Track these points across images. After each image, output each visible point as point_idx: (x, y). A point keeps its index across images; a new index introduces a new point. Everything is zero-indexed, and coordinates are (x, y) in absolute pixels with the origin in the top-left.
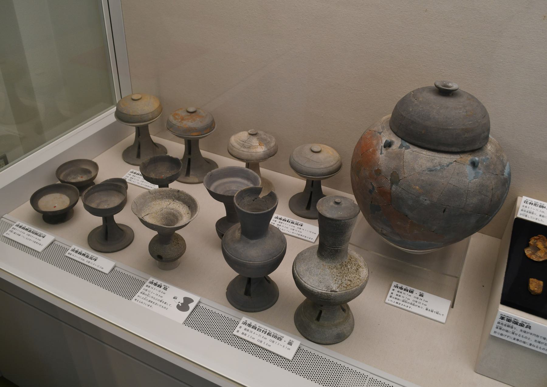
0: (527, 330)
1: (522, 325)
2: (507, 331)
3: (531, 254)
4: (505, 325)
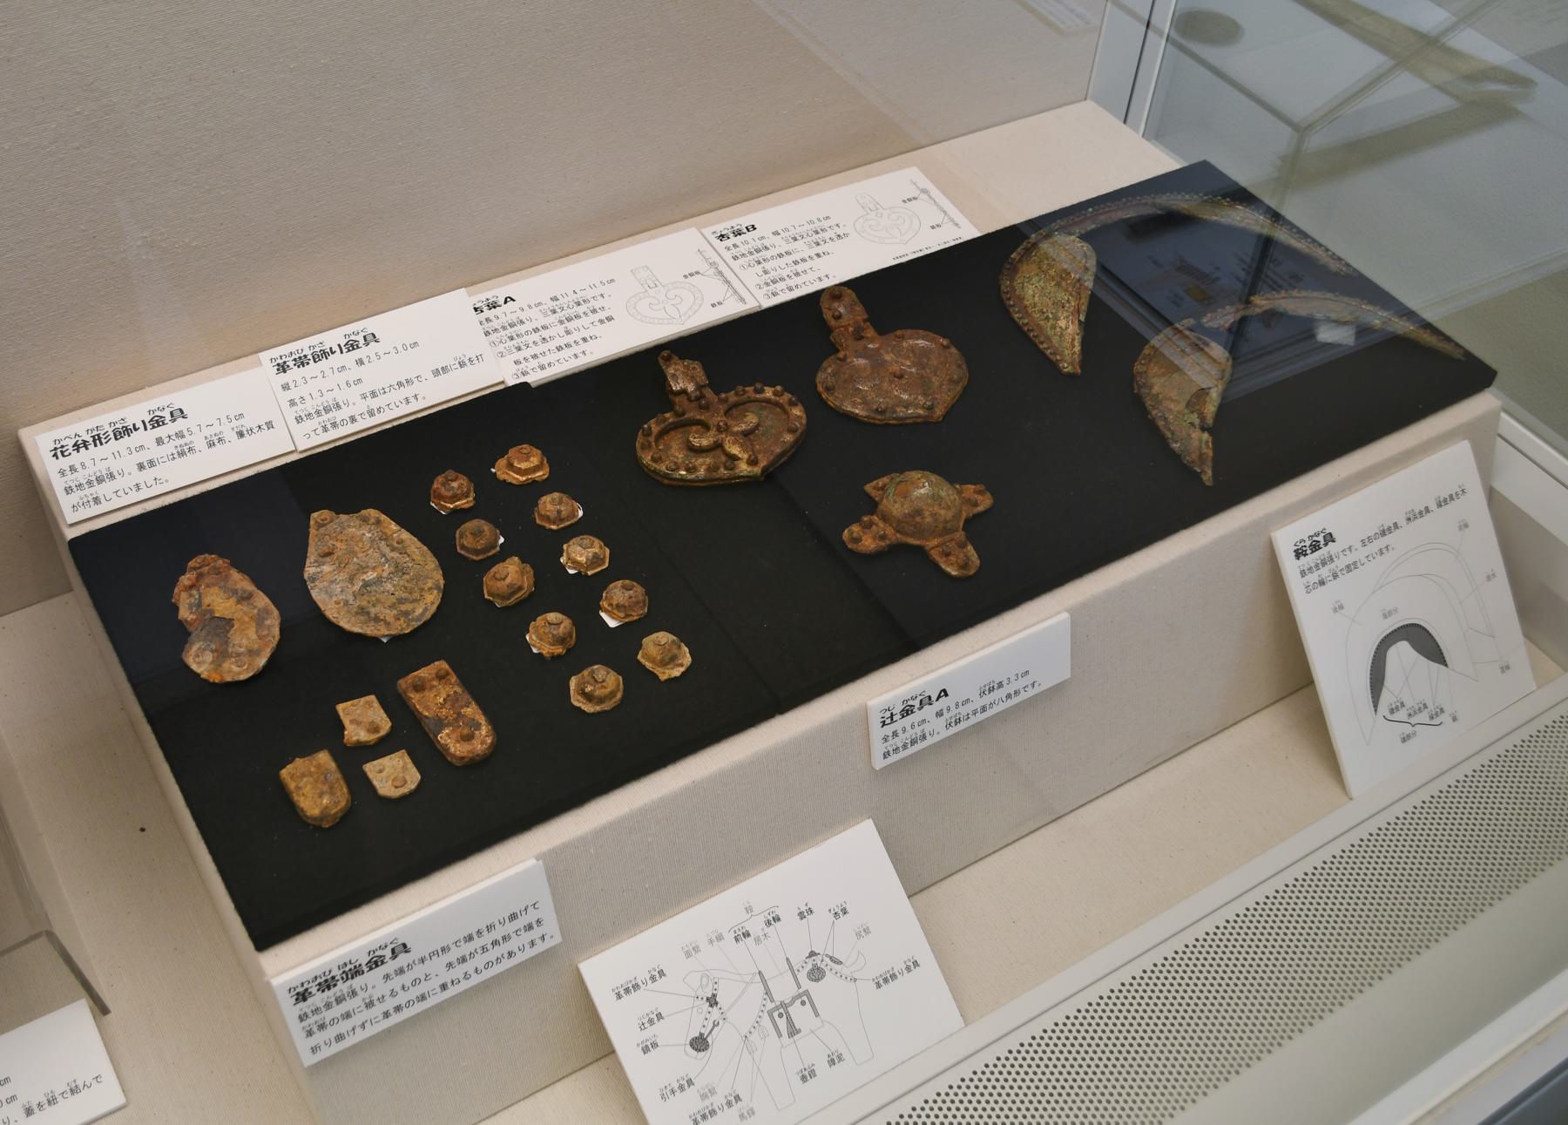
0: (403, 959)
1: (376, 962)
2: (347, 1015)
3: (217, 664)
4: (328, 1006)
